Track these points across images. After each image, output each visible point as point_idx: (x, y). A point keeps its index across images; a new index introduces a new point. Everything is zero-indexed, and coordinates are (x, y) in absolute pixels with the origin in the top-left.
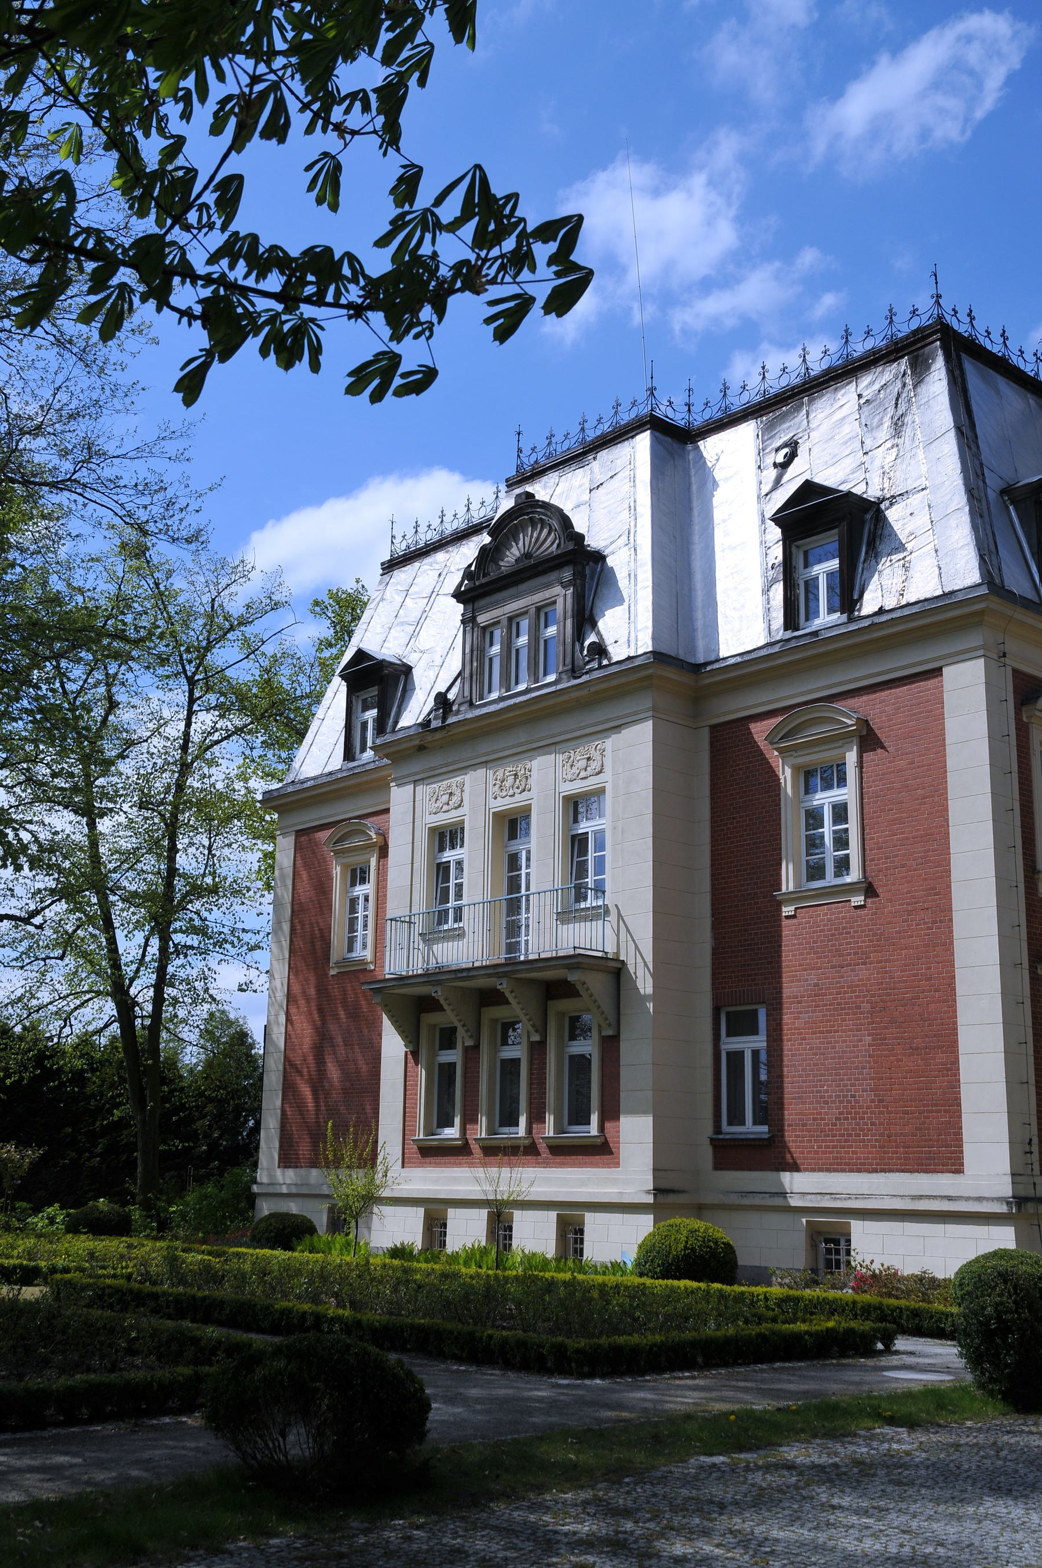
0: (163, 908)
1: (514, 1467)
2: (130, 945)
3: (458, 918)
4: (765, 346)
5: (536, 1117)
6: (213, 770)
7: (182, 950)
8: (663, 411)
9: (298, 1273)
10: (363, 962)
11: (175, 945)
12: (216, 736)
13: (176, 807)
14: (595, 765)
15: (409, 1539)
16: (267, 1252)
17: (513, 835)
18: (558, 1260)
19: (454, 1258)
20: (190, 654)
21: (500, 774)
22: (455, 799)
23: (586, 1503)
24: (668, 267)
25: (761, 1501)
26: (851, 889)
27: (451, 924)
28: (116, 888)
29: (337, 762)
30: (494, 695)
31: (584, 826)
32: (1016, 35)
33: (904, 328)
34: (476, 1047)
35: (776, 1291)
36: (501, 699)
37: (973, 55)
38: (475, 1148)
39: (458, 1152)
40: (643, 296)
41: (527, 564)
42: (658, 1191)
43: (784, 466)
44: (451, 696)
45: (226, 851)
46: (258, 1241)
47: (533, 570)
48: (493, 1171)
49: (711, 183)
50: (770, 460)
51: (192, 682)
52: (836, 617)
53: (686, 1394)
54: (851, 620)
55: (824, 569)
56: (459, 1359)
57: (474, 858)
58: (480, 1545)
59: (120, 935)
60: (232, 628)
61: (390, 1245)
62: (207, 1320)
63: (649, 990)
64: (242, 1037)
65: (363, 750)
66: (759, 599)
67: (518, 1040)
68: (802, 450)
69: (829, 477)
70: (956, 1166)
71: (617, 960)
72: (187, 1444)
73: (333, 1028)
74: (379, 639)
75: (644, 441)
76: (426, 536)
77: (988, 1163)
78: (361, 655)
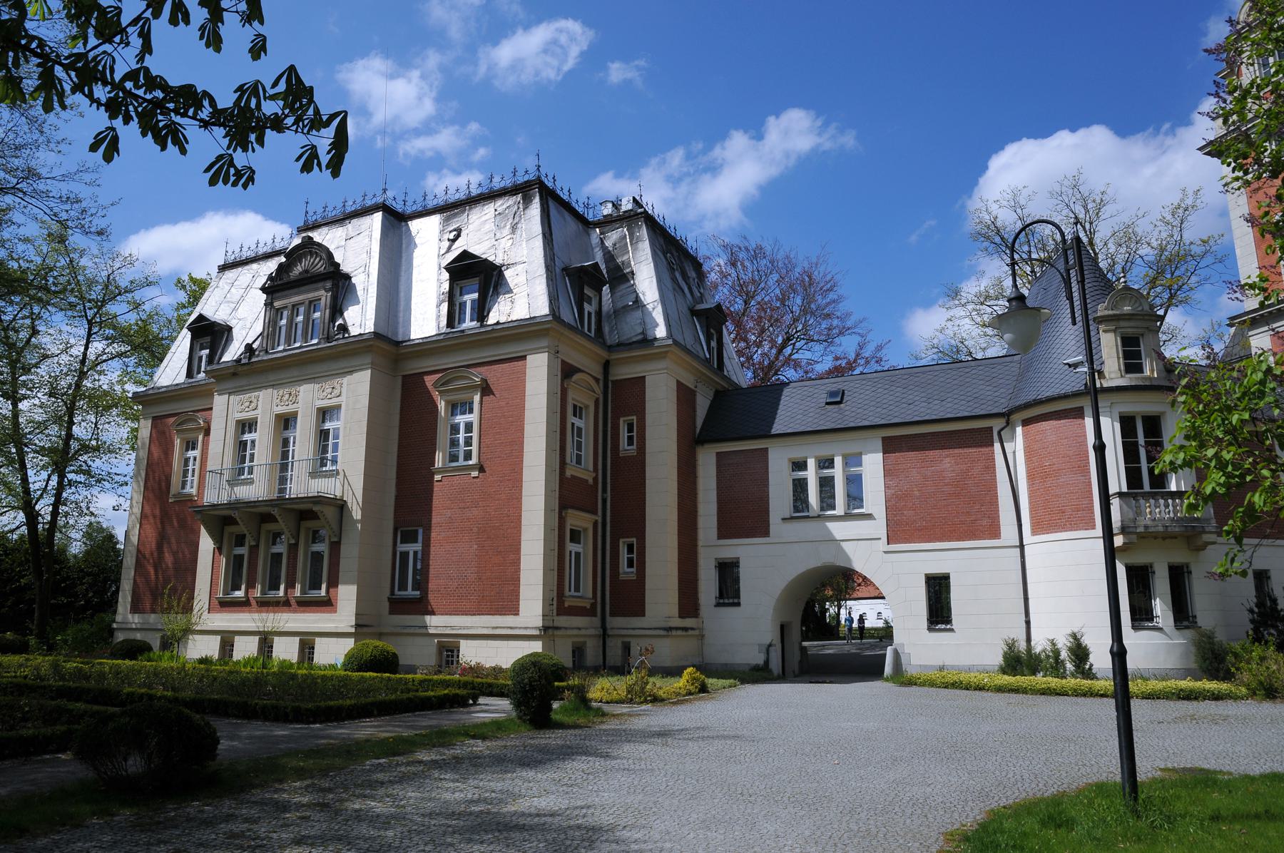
0: (61, 459)
1: (268, 770)
2: (37, 479)
3: (251, 472)
4: (445, 171)
5: (290, 585)
6: (102, 377)
7: (70, 483)
8: (390, 202)
9: (139, 672)
10: (191, 495)
11: (70, 481)
12: (105, 357)
13: (75, 397)
14: (336, 392)
15: (202, 811)
16: (120, 661)
17: (286, 428)
18: (298, 663)
19: (238, 662)
20: (94, 304)
21: (281, 392)
22: (253, 405)
23: (307, 786)
24: (396, 118)
25: (403, 779)
26: (472, 468)
27: (245, 476)
28: (31, 442)
29: (181, 378)
30: (281, 348)
31: (328, 425)
32: (584, 33)
33: (521, 179)
34: (257, 546)
35: (419, 676)
36: (285, 350)
37: (563, 39)
38: (253, 602)
39: (243, 604)
40: (383, 132)
41: (305, 277)
42: (357, 626)
43: (453, 241)
44: (255, 346)
45: (107, 426)
46: (113, 656)
47: (309, 280)
48: (264, 615)
49: (423, 77)
50: (446, 236)
51: (90, 323)
52: (474, 323)
53: (366, 730)
54: (482, 326)
55: (470, 298)
56: (237, 717)
57: (262, 439)
58: (244, 811)
59: (30, 473)
60: (120, 294)
61: (198, 657)
62: (77, 700)
63: (359, 517)
64: (110, 538)
65: (199, 372)
66: (434, 310)
67: (281, 543)
69: (476, 250)
70: (515, 612)
71: (342, 500)
72: (65, 767)
73: (169, 531)
74: (213, 310)
75: (378, 216)
76: (246, 254)
77: (532, 609)
78: (201, 317)
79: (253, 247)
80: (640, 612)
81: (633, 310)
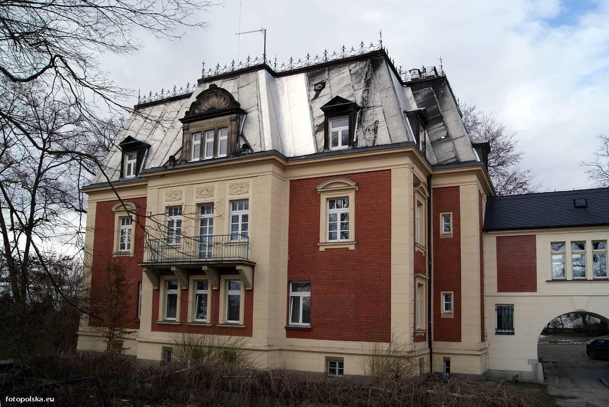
34: (187, 290)
44: (177, 157)
68: (327, 85)
79: (159, 93)
80: (458, 338)
81: (446, 142)
